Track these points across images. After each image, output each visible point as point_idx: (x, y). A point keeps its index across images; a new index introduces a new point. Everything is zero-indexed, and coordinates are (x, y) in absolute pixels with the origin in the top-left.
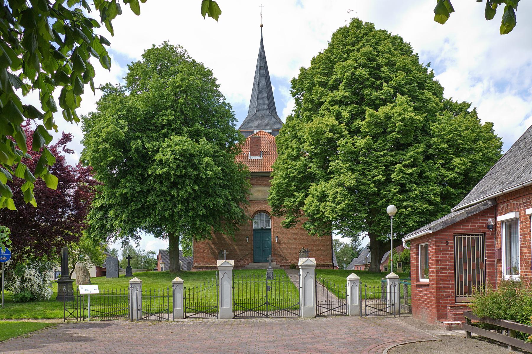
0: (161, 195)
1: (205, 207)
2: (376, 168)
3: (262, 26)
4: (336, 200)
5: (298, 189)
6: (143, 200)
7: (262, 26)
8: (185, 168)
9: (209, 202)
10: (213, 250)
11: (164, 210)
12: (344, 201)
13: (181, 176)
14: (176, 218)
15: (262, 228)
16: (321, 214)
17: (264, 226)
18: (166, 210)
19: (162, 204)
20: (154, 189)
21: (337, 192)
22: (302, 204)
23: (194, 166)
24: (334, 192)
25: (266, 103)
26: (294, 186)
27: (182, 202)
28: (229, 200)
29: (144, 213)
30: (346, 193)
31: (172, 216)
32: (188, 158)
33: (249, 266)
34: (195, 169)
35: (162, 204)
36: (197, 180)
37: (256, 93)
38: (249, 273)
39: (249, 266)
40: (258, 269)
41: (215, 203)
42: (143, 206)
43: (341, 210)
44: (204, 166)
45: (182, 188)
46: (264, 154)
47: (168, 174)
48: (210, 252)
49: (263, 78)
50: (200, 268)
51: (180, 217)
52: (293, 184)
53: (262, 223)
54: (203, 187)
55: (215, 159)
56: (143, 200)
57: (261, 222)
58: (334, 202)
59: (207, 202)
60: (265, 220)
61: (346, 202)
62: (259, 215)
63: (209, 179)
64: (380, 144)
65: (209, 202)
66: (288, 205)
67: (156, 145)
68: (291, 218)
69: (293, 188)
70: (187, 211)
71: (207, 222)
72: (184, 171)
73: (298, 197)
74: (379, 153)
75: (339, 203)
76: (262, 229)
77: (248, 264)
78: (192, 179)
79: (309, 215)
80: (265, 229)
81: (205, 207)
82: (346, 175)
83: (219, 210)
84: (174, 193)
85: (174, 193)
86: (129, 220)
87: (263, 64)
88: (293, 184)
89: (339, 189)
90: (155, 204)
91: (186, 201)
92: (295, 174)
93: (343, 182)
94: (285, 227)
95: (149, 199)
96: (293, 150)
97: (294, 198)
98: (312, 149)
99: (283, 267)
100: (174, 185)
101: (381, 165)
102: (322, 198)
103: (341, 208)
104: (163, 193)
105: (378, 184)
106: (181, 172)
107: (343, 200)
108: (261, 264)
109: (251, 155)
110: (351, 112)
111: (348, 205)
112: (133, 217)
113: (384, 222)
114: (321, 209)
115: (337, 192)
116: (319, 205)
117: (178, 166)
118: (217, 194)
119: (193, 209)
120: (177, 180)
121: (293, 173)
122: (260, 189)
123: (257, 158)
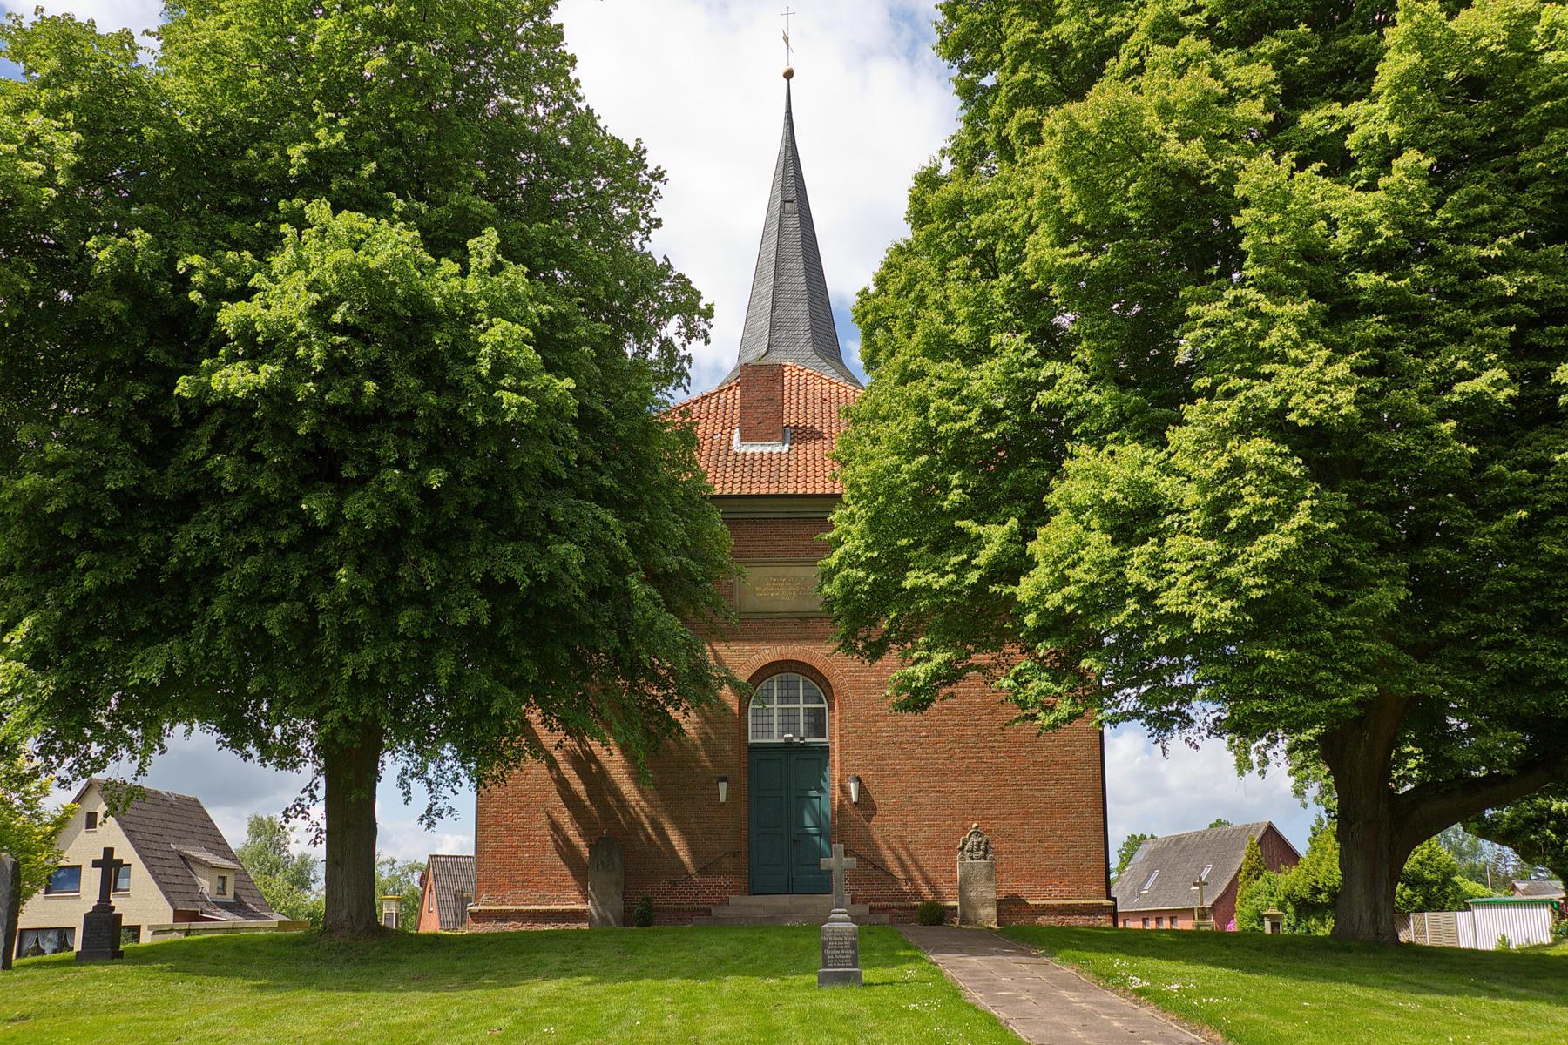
0: (252, 518)
1: (488, 587)
2: (1459, 335)
3: (789, 75)
4: (1235, 513)
5: (983, 508)
6: (145, 543)
7: (789, 75)
8: (377, 371)
9: (511, 562)
10: (567, 840)
11: (258, 596)
12: (1284, 518)
13: (356, 418)
14: (328, 645)
15: (789, 743)
16: (1132, 605)
17: (796, 732)
18: (274, 600)
19: (250, 567)
20: (212, 490)
21: (1237, 467)
22: (1013, 567)
23: (431, 369)
24: (1223, 462)
25: (805, 321)
26: (963, 487)
27: (361, 557)
28: (619, 568)
29: (155, 615)
30: (1293, 468)
31: (306, 631)
32: (396, 329)
33: (726, 911)
34: (441, 387)
35: (250, 567)
36: (447, 440)
37: (767, 288)
38: (719, 945)
39: (726, 911)
40: (773, 921)
41: (542, 568)
42: (148, 575)
43: (1271, 569)
44: (485, 367)
45: (362, 482)
46: (802, 435)
47: (278, 397)
48: (551, 846)
49: (794, 240)
50: (504, 916)
51: (350, 640)
52: (955, 479)
53: (789, 718)
54: (479, 481)
55: (554, 357)
56: (145, 543)
57: (785, 713)
58: (1214, 529)
59: (500, 563)
60: (802, 706)
61: (1301, 518)
62: (774, 685)
63: (503, 433)
64: (1475, 201)
65: (511, 562)
66: (928, 589)
67: (237, 267)
68: (939, 657)
69: (955, 496)
70: (386, 609)
71: (497, 675)
72: (371, 387)
73: (978, 542)
74: (1475, 251)
75: (1249, 531)
76: (788, 744)
77: (724, 902)
78: (415, 435)
79: (1055, 624)
80: (805, 748)
81: (488, 587)
82: (1300, 364)
83: (562, 613)
84: (314, 506)
85: (314, 506)
86: (64, 641)
87: (792, 195)
88: (955, 479)
89: (1256, 449)
90: (214, 568)
91: (384, 546)
92: (966, 424)
93: (1274, 403)
94: (905, 707)
95: (184, 539)
96: (950, 317)
97: (958, 552)
98: (1073, 255)
99: (886, 917)
100: (319, 465)
101: (1485, 316)
102: (1136, 520)
103: (1273, 554)
104: (261, 512)
105: (1479, 419)
106: (358, 392)
107: (1276, 509)
108: (784, 901)
109: (744, 439)
110: (1279, 60)
111: (1310, 541)
112: (91, 633)
113: (1506, 646)
114: (1134, 576)
115: (1237, 467)
116: (1120, 561)
117: (337, 366)
118: (552, 526)
119: (422, 599)
120: (332, 437)
121: (960, 417)
122: (781, 571)
123: (767, 450)
